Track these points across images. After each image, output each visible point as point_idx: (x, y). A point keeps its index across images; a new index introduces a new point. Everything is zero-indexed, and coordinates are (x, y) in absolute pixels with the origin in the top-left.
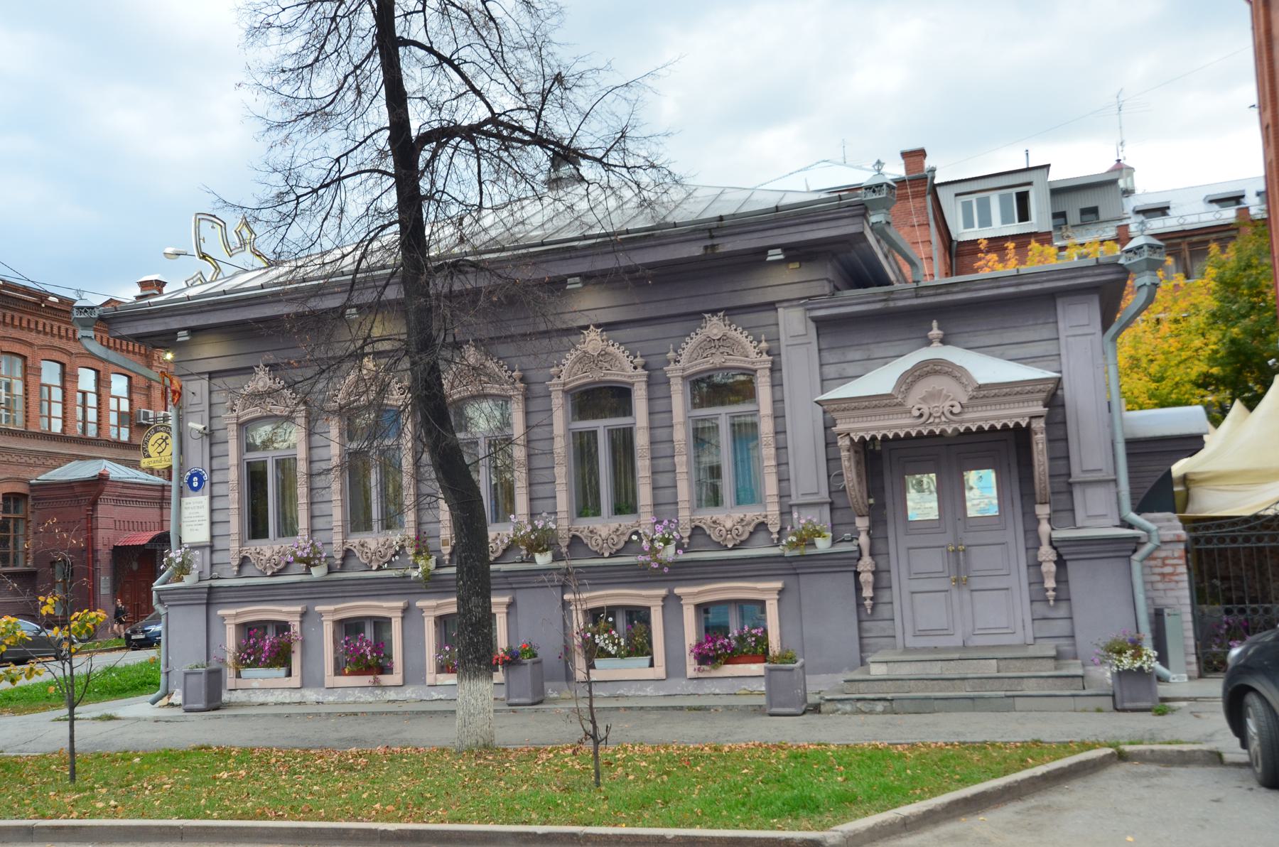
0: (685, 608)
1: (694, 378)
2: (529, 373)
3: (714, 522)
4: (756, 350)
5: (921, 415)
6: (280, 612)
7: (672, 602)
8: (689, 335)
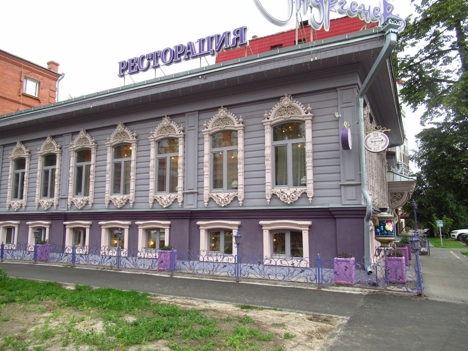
0: (201, 230)
1: (274, 126)
2: (245, 121)
3: (282, 192)
4: (237, 122)
7: (133, 229)
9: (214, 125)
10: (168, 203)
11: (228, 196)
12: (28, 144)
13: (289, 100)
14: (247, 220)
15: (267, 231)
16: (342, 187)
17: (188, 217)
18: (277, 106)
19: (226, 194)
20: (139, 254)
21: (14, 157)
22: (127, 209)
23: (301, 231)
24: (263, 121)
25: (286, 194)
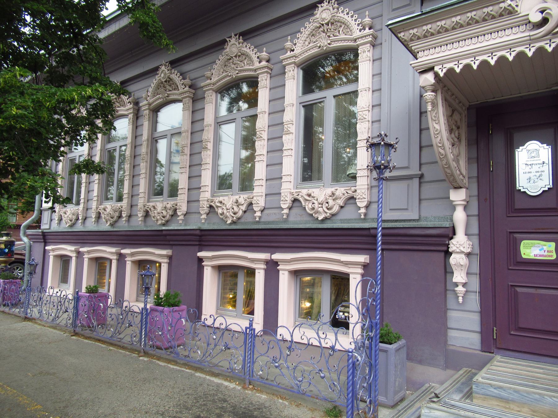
0: (281, 272)
2: (272, 56)
4: (360, 27)
6: (153, 254)
8: (299, 31)
9: (307, 43)
10: (328, 209)
11: (333, 194)
12: (187, 67)
13: (331, 8)
14: (416, 254)
15: (286, 273)
17: (197, 243)
18: (309, 26)
20: (125, 304)
21: (219, 80)
22: (247, 224)
23: (348, 275)
24: (282, 57)
25: (317, 200)
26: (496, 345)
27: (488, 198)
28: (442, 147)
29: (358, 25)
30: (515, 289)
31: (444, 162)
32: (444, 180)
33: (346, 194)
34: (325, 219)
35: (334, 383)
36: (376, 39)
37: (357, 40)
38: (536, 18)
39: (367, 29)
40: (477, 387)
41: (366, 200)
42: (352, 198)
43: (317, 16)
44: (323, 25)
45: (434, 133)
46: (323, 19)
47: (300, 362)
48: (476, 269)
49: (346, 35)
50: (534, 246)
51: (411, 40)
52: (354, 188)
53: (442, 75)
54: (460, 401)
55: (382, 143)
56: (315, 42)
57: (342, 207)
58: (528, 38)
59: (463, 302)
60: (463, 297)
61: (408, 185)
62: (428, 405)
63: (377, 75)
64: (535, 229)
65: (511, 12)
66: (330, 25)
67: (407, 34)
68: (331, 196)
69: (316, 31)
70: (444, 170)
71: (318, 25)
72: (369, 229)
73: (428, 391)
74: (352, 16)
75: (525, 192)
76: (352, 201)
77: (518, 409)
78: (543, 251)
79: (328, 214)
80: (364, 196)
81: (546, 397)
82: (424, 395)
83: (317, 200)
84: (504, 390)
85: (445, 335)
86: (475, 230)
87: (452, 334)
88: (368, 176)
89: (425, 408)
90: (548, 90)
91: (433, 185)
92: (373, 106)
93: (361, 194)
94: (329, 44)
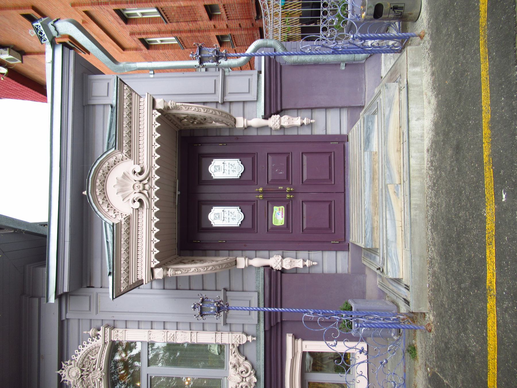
4: (95, 339)
5: (140, 201)
10: (247, 372)
11: (234, 366)
13: (69, 367)
16: (229, 321)
19: (232, 371)
25: (239, 383)
26: (343, 242)
27: (244, 244)
28: (207, 268)
29: (93, 340)
30: (305, 230)
31: (218, 267)
32: (230, 270)
33: (236, 354)
34: (256, 375)
35: (389, 351)
36: (109, 326)
37: (106, 341)
38: (137, 205)
39: (99, 332)
40: (368, 245)
41: (241, 335)
42: (238, 348)
43: (72, 381)
44: (82, 376)
45: (197, 272)
46: (77, 375)
47: (379, 384)
48: (293, 253)
49: (97, 353)
50: (276, 218)
51: (128, 282)
52: (230, 345)
53: (158, 262)
54: (379, 256)
55: (201, 304)
56: (95, 385)
57: (246, 359)
58: (148, 210)
59: (316, 262)
60: (313, 262)
61: (231, 300)
62: (386, 273)
63: (139, 324)
64: (266, 217)
65: (128, 219)
66: (84, 369)
67: (123, 285)
68: (236, 369)
69: (85, 384)
70: (223, 268)
71: (81, 380)
72: (265, 331)
73: (382, 284)
74: (83, 346)
75: (241, 222)
76: (241, 349)
77: (376, 222)
78: (279, 213)
79: (252, 372)
80: (238, 337)
81: (365, 208)
82: (384, 285)
83: (239, 383)
84: (367, 229)
85: (341, 275)
86: (266, 253)
87: (340, 271)
88: (222, 333)
89: (388, 275)
90: (177, 208)
91: (233, 282)
92: (164, 329)
93: (236, 339)
94: (101, 369)
